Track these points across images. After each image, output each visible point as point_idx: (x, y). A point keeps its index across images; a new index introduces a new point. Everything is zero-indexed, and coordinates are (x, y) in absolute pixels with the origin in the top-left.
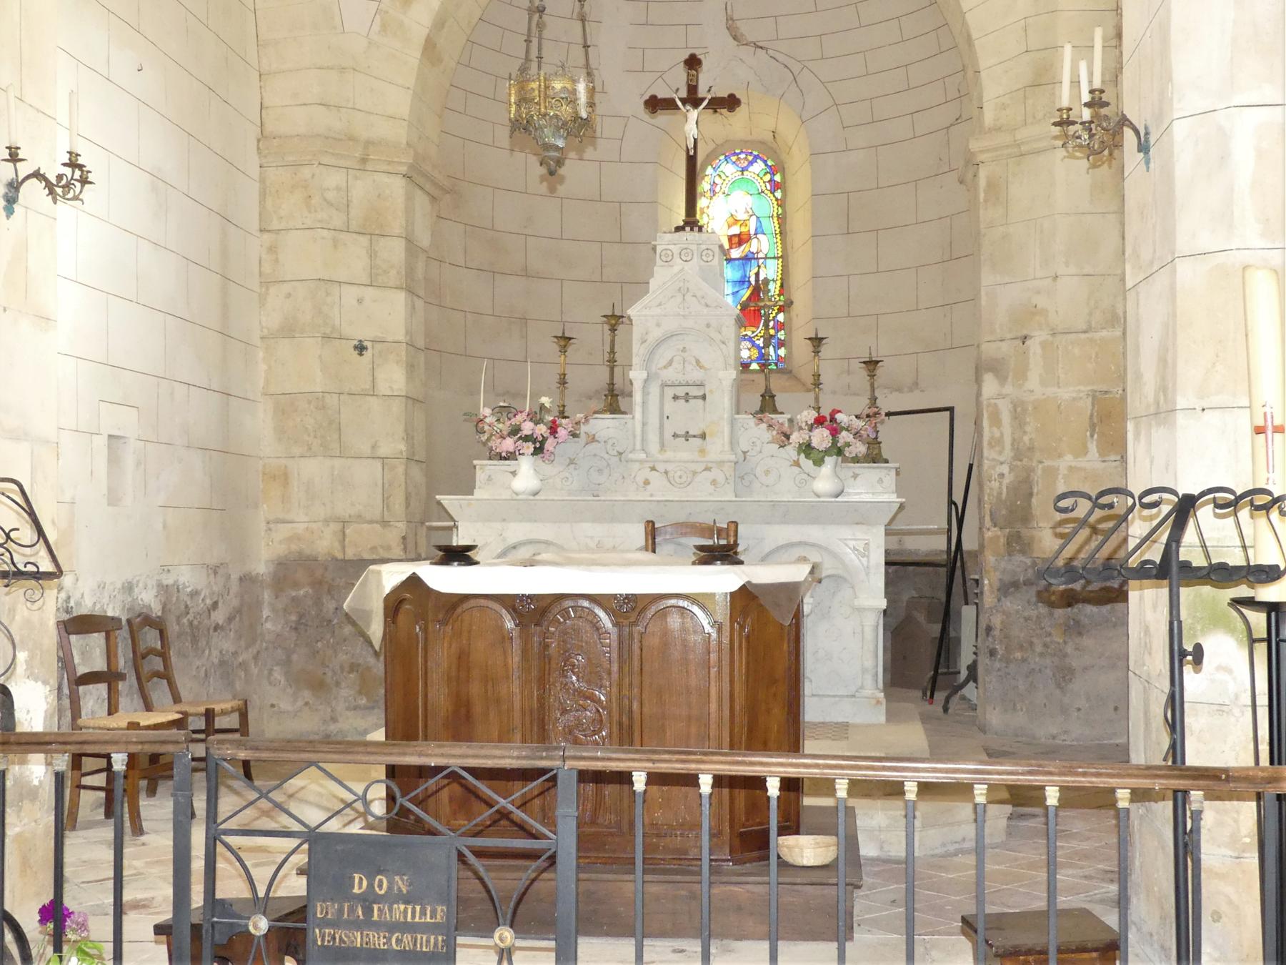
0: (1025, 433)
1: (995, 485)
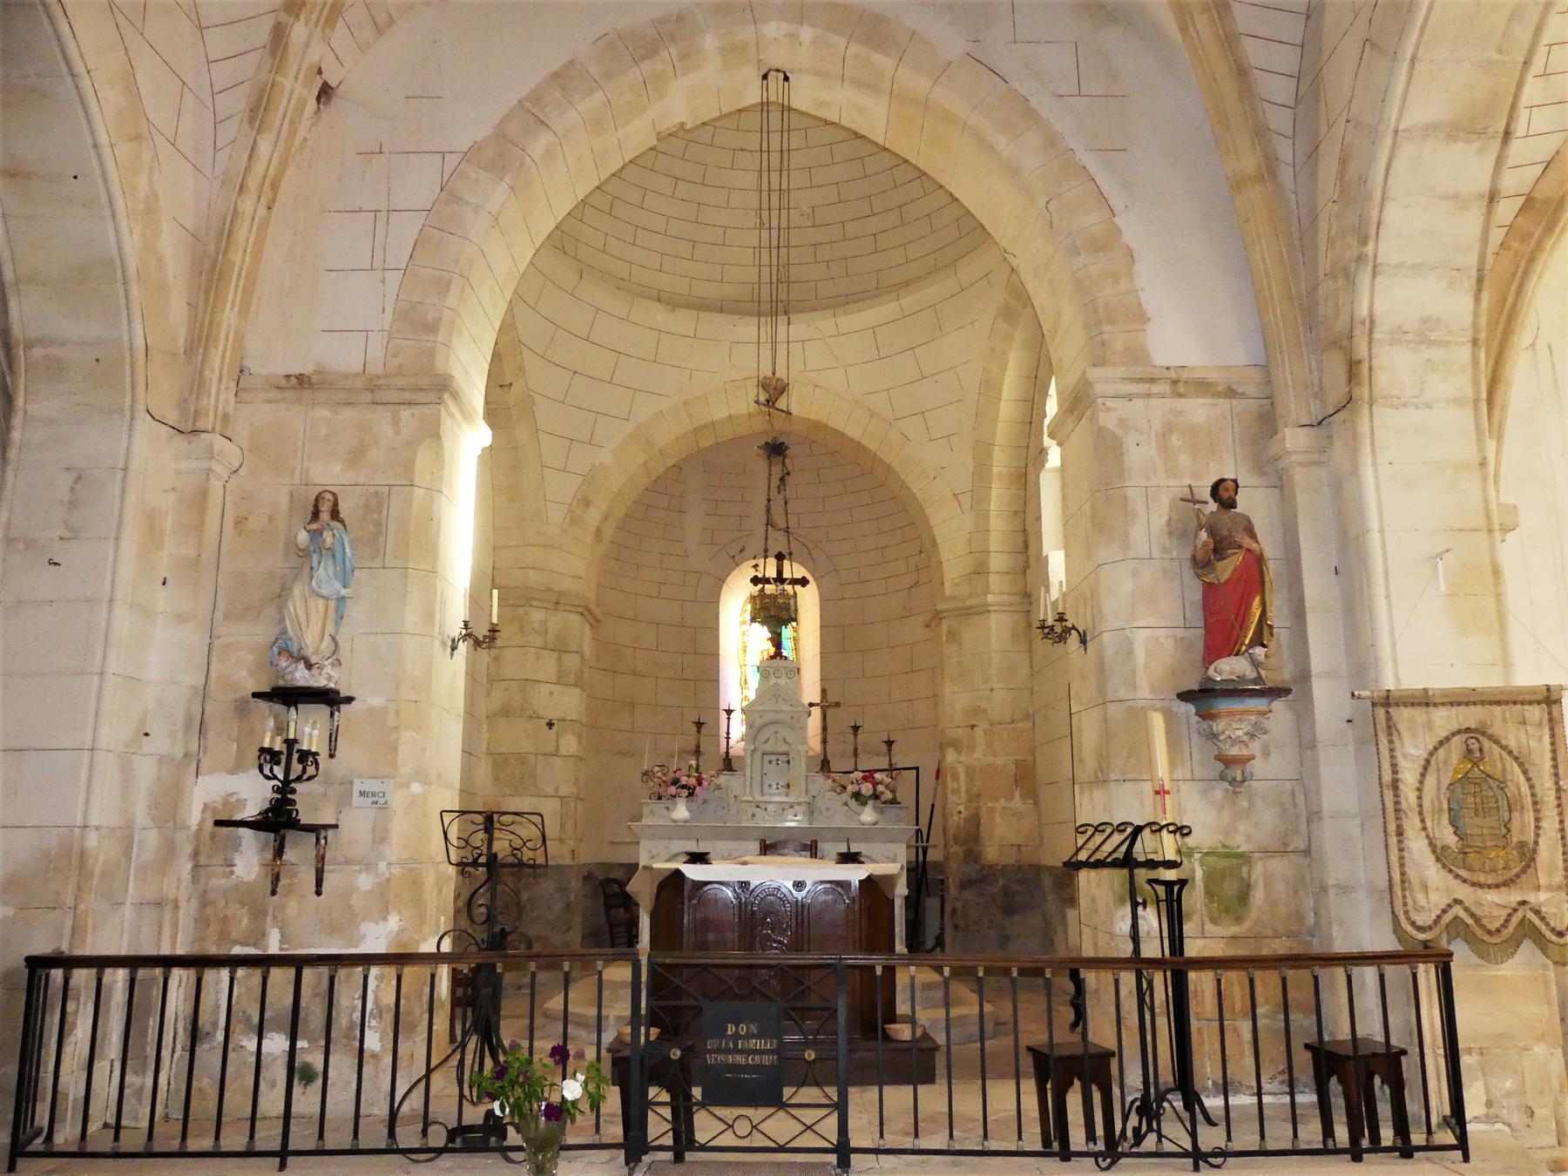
0: (974, 786)
1: (956, 818)
